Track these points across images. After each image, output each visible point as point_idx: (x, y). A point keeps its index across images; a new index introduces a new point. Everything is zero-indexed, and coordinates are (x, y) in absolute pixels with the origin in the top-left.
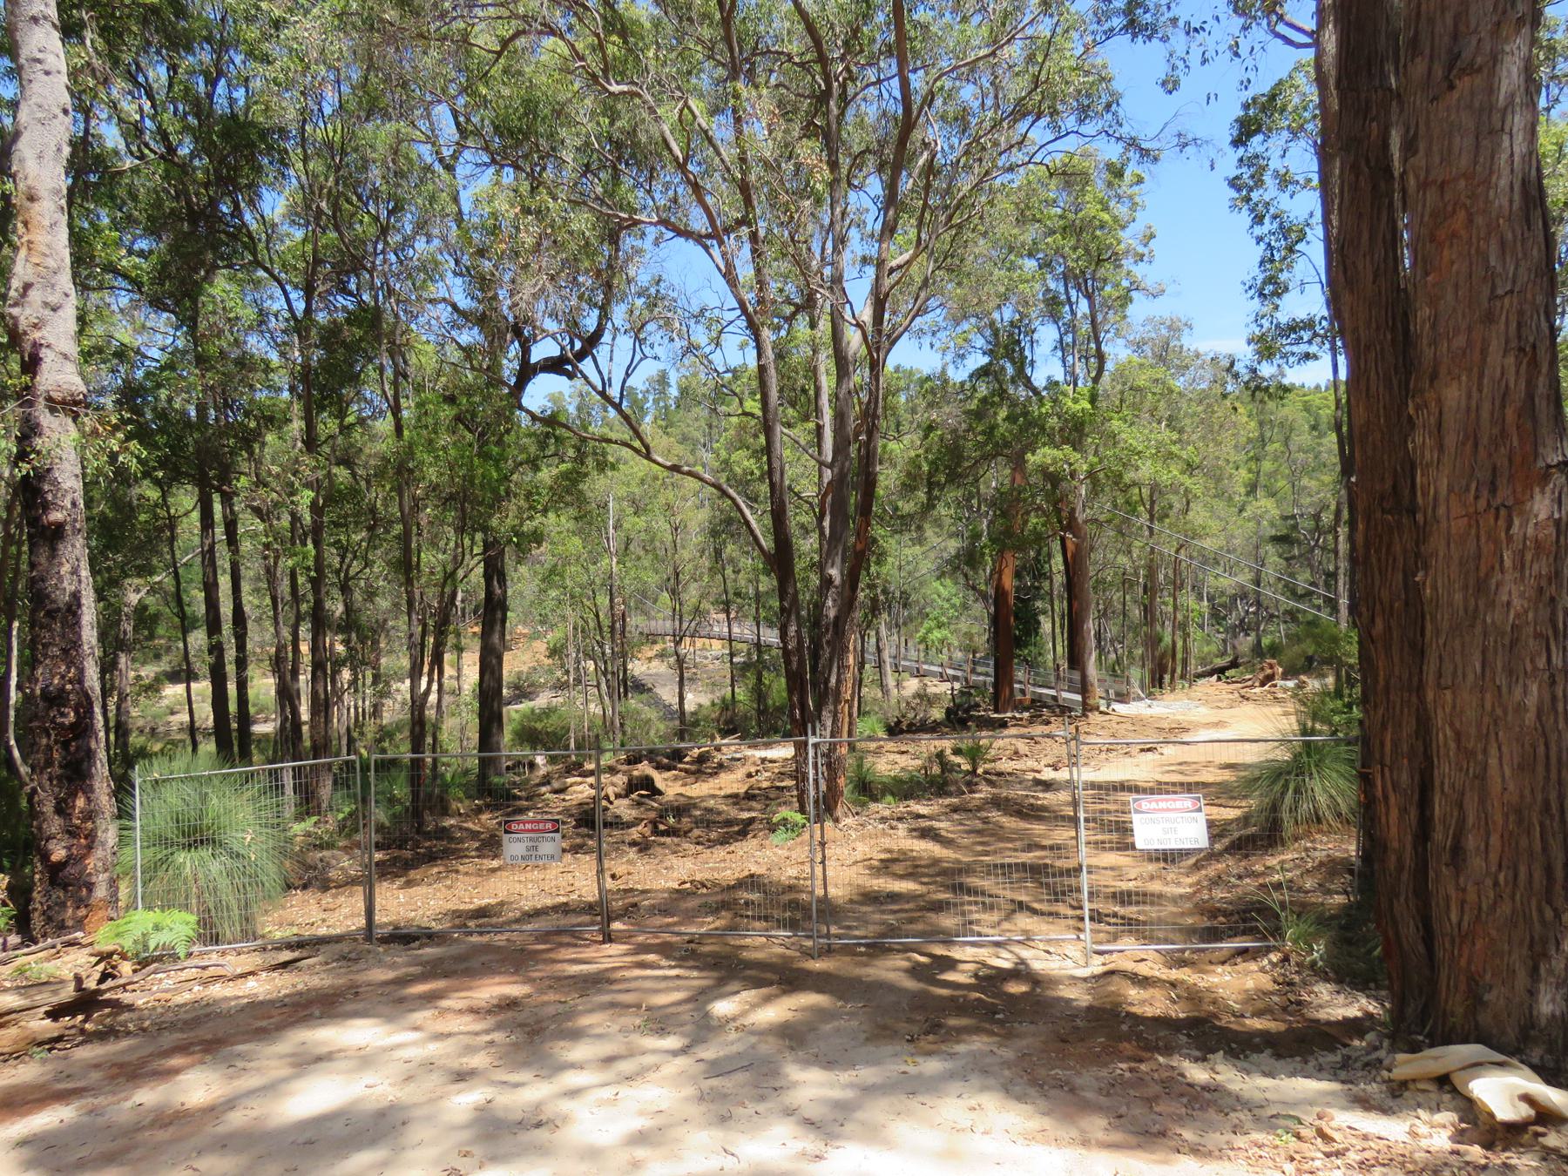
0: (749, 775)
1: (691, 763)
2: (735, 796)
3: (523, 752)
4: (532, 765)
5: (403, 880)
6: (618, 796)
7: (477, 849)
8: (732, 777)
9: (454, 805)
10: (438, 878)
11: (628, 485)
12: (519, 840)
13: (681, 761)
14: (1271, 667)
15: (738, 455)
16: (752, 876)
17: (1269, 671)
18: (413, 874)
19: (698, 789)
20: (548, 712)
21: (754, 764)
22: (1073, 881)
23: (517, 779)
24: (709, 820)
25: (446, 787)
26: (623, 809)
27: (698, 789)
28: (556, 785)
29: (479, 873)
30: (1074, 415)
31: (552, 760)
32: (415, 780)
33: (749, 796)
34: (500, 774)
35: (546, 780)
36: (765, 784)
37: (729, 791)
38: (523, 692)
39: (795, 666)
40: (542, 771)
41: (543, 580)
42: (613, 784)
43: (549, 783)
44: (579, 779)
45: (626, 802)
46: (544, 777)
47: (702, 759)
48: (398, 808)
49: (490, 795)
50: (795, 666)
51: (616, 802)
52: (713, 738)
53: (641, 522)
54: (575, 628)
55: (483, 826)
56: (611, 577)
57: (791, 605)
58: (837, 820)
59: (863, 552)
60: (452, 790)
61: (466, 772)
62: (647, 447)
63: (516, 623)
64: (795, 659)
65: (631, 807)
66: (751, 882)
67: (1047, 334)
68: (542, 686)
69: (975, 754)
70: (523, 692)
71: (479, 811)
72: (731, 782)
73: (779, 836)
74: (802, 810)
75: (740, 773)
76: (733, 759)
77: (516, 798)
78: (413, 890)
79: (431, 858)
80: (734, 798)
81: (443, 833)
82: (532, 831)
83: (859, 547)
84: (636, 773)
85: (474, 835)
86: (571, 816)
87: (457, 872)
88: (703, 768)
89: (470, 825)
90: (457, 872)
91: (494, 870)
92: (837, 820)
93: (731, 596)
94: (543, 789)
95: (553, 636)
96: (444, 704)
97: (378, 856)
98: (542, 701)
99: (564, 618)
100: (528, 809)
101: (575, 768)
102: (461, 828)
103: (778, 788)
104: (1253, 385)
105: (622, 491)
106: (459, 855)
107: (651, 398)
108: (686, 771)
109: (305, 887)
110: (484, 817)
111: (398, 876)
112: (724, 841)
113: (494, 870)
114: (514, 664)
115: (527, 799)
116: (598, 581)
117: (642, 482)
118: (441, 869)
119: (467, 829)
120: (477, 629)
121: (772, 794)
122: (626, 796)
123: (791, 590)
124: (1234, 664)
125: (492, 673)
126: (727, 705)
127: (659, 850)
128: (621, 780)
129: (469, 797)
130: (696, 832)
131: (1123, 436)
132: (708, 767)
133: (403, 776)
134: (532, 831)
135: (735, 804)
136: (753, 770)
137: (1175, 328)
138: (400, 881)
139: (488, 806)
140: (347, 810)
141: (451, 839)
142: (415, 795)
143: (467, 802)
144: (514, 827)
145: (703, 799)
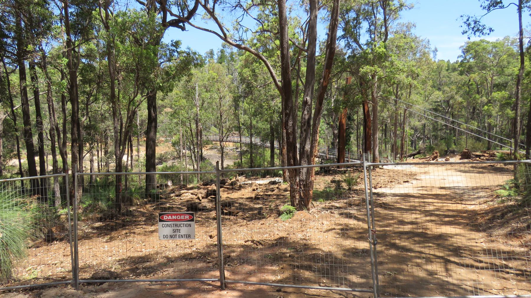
0: (254, 190)
1: (229, 185)
2: (251, 198)
3: (164, 182)
4: (167, 186)
5: (109, 236)
6: (203, 198)
7: (145, 221)
8: (246, 191)
9: (135, 201)
10: (126, 235)
11: (203, 80)
12: (168, 226)
13: (224, 185)
14: (436, 153)
15: (245, 70)
16: (281, 238)
17: (436, 155)
18: (114, 234)
19: (235, 195)
20: (172, 167)
21: (256, 185)
22: (39, 181)
23: (161, 191)
24: (242, 208)
25: (131, 193)
26: (205, 203)
27: (235, 195)
28: (177, 193)
29: (146, 234)
30: (379, 53)
31: (174, 184)
32: (117, 190)
33: (257, 198)
34: (154, 188)
35: (173, 191)
36: (262, 194)
37: (248, 197)
38: (162, 160)
39: (291, 140)
40: (171, 188)
41: (171, 116)
42: (201, 193)
43: (174, 192)
44: (185, 191)
45: (206, 200)
46: (172, 190)
47: (232, 184)
48: (110, 202)
49: (150, 197)
50: (291, 140)
51: (203, 200)
52: (236, 177)
53: (208, 95)
54: (183, 135)
55: (148, 210)
56: (197, 115)
57: (290, 112)
58: (308, 210)
59: (326, 86)
60: (134, 195)
61: (141, 188)
62: (225, 34)
63: (160, 137)
64: (291, 137)
65: (208, 202)
66: (282, 242)
67: (365, 25)
68: (169, 159)
69: (350, 182)
70: (162, 160)
71: (146, 203)
72: (247, 193)
73: (284, 217)
74: (293, 205)
75: (250, 189)
76: (244, 184)
77: (161, 198)
78: (112, 243)
79: (124, 226)
80: (250, 199)
81: (129, 214)
82: (174, 220)
83: (325, 84)
84: (210, 189)
85: (143, 214)
86: (184, 206)
87: (134, 233)
88: (234, 187)
89: (142, 210)
90: (134, 233)
91: (152, 232)
92: (308, 210)
93: (241, 125)
94: (172, 195)
95: (175, 138)
96: (133, 164)
97: (97, 224)
98: (169, 163)
99: (179, 131)
100: (166, 203)
101: (184, 187)
102: (138, 211)
103: (267, 195)
104: (475, 29)
105: (201, 83)
106: (136, 223)
107: (207, 59)
108: (228, 188)
109: (61, 240)
110: (148, 206)
111: (106, 235)
112: (252, 218)
113: (152, 232)
114: (160, 150)
115: (166, 199)
116: (192, 117)
117: (209, 80)
118: (127, 231)
119: (140, 212)
120: (145, 139)
121: (265, 197)
122: (206, 198)
123: (290, 105)
124: (419, 153)
125: (151, 148)
126: (239, 165)
127: (228, 223)
128: (204, 192)
129: (142, 198)
130: (240, 214)
131: (395, 63)
132: (237, 186)
133: (113, 189)
134: (174, 220)
135: (251, 201)
136: (255, 188)
137: (409, 27)
138: (107, 238)
139: (149, 201)
140: (87, 203)
141: (134, 216)
142: (117, 196)
143: (141, 200)
144: (165, 217)
145: (238, 199)
